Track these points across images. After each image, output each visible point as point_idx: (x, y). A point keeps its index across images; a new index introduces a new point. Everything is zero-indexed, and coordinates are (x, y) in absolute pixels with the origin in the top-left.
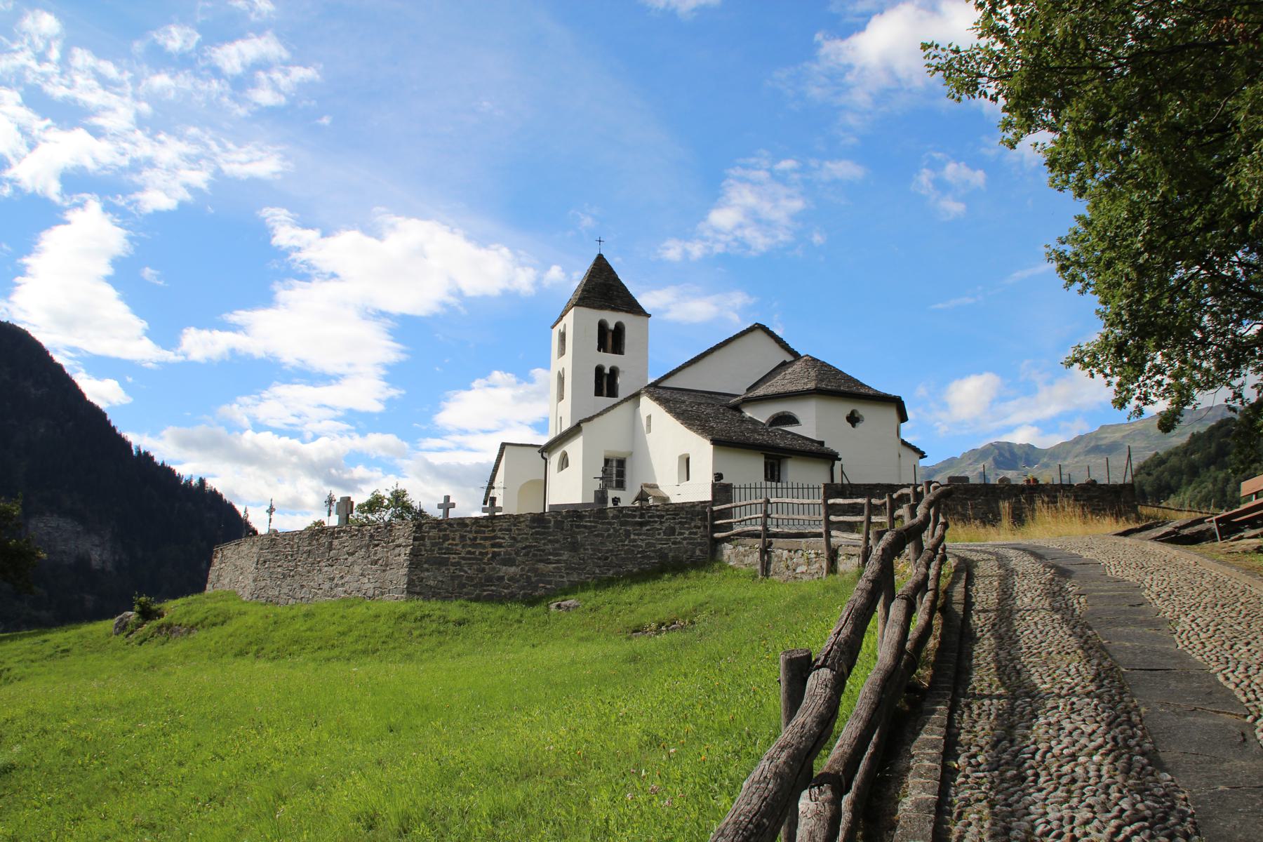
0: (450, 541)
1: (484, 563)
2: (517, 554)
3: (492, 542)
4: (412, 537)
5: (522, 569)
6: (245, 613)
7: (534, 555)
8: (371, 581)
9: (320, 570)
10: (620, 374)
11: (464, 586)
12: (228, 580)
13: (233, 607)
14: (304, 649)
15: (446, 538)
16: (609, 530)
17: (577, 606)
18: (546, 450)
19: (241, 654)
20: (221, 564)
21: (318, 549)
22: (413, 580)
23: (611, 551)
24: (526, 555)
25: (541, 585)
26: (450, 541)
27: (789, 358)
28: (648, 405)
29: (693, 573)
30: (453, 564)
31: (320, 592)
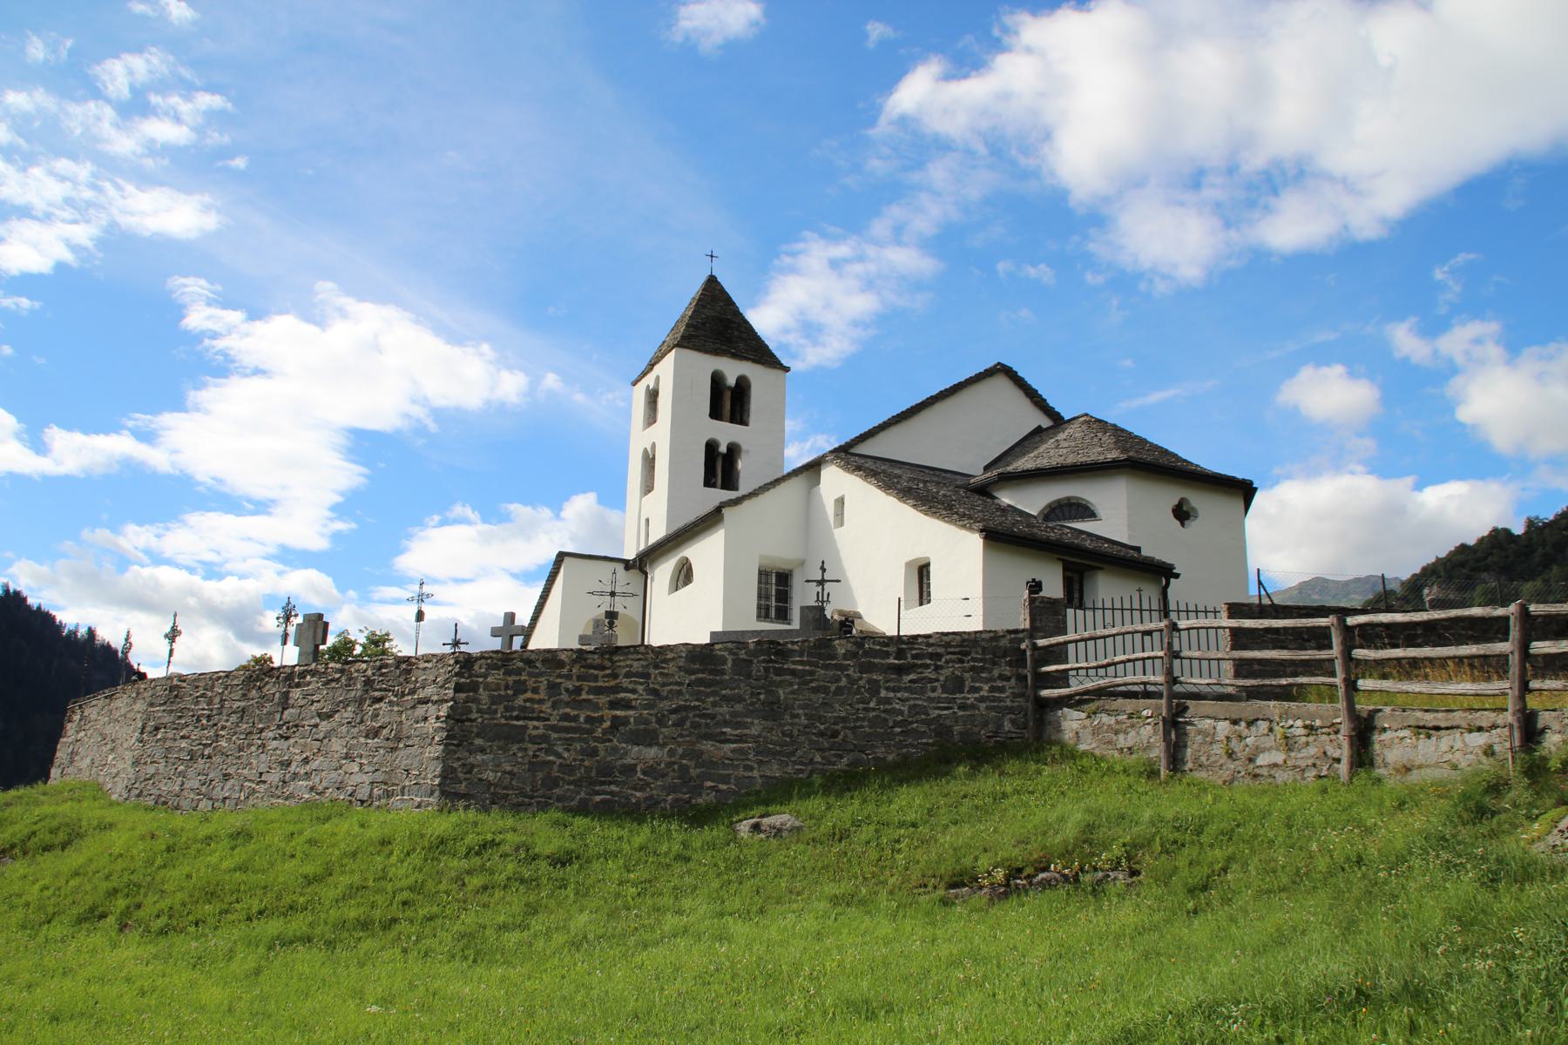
0: (529, 695)
1: (596, 739)
2: (661, 721)
3: (612, 697)
4: (452, 685)
5: (671, 753)
6: (111, 826)
7: (695, 726)
8: (366, 768)
9: (263, 746)
10: (743, 455)
11: (555, 783)
12: (88, 761)
13: (91, 812)
14: (227, 912)
15: (520, 688)
16: (838, 680)
17: (799, 829)
18: (642, 564)
19: (93, 916)
20: (78, 732)
21: (260, 706)
22: (454, 770)
23: (844, 720)
24: (679, 724)
25: (709, 784)
26: (529, 695)
27: (1046, 422)
28: (835, 479)
29: (1012, 766)
30: (533, 740)
31: (262, 787)
